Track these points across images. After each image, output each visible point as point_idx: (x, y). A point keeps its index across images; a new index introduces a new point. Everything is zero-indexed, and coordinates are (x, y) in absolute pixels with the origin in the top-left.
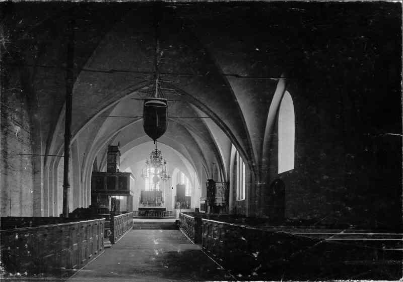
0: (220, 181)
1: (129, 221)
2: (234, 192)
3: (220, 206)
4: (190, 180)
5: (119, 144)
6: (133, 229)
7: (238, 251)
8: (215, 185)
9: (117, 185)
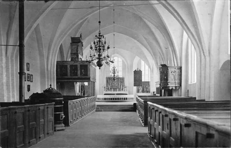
0: (173, 66)
1: (92, 104)
2: (187, 76)
3: (172, 89)
4: (149, 67)
5: (81, 35)
6: (96, 111)
7: (213, 70)
8: (168, 69)
9: (79, 72)
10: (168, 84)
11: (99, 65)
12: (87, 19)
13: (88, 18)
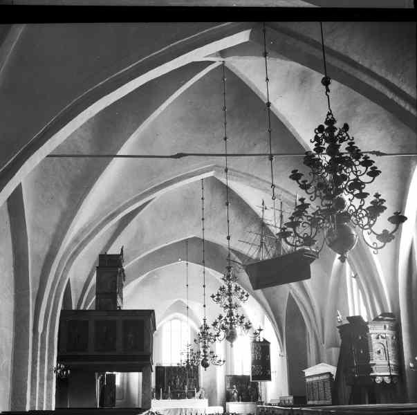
9: (119, 344)
10: (372, 371)
11: (206, 365)
12: (149, 201)
13: (69, 280)
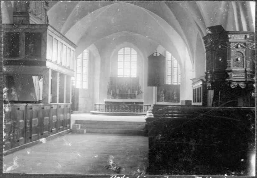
10: (228, 76)
